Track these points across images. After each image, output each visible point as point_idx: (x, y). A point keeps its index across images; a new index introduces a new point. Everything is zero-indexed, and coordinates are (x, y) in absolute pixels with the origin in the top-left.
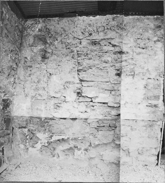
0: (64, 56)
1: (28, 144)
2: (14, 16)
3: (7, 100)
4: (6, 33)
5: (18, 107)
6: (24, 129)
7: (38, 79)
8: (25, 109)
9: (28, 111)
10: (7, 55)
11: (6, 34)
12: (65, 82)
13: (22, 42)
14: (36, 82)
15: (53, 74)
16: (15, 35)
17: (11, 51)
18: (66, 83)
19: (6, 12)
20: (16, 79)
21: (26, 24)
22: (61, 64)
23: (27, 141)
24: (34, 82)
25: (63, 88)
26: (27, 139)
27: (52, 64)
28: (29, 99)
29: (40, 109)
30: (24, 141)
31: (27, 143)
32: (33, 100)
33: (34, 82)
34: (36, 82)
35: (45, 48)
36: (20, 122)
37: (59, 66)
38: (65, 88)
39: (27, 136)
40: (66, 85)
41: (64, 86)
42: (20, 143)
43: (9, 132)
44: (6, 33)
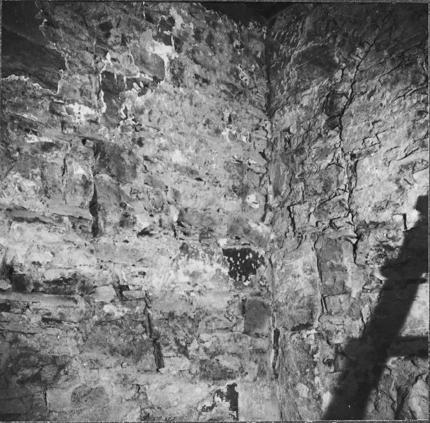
0: (389, 87)
1: (317, 379)
2: (220, 21)
3: (245, 252)
4: (196, 75)
5: (283, 270)
6: (305, 333)
7: (322, 183)
8: (300, 271)
9: (309, 277)
10: (218, 132)
11: (197, 76)
12: (398, 170)
13: (271, 89)
14: (320, 191)
15: (360, 155)
16: (238, 72)
17: (230, 120)
18: (401, 171)
19: (184, 17)
20: (271, 197)
21: (273, 34)
22: (382, 117)
23: (316, 371)
24: (316, 193)
25: (396, 188)
26: (315, 364)
27: (355, 124)
28: (308, 244)
29: (339, 266)
30: (308, 370)
31: (314, 376)
32: (319, 246)
33: (316, 193)
34: (320, 191)
35: (330, 85)
36: (294, 312)
37: (376, 125)
38: (401, 187)
39: (315, 353)
40: (402, 179)
41: (397, 181)
42: (298, 377)
43: (262, 343)
44: (196, 75)
